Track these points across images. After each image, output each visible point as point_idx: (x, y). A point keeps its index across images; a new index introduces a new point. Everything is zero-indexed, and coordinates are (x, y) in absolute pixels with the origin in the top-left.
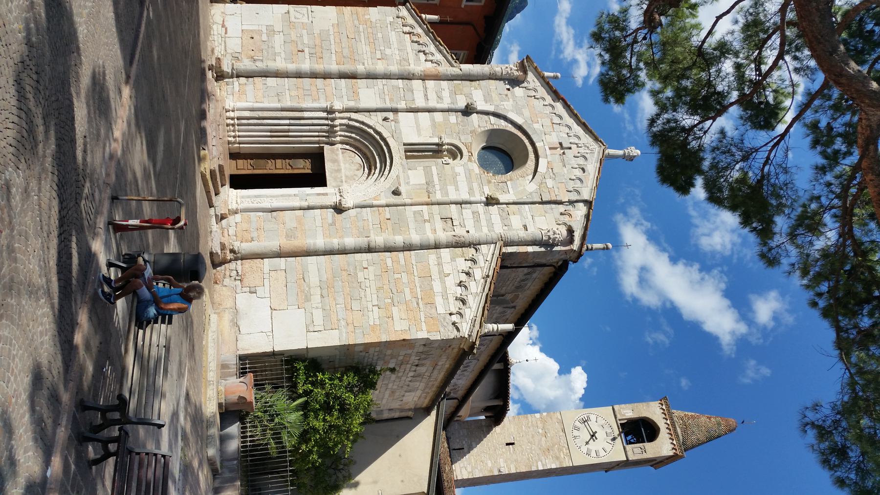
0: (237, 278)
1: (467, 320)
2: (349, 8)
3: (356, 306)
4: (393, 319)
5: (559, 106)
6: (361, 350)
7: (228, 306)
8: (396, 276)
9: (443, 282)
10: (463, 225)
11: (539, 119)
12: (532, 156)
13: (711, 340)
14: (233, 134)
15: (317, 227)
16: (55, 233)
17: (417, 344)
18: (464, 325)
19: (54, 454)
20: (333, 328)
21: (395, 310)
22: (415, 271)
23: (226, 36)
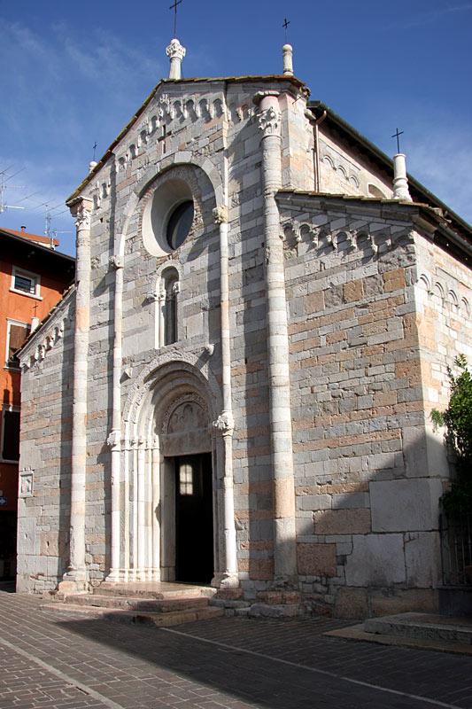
0: (324, 582)
1: (386, 226)
2: (22, 426)
3: (364, 403)
4: (386, 343)
5: (118, 152)
6: (436, 392)
7: (364, 598)
8: (323, 342)
9: (333, 271)
10: (255, 253)
11: (133, 174)
12: (173, 175)
13: (419, 232)
14: (150, 573)
15: (255, 465)
16: (458, 263)
17: (427, 304)
18: (394, 230)
19: (444, 449)
20: (350, 540)
21: (372, 341)
22: (316, 315)
23: (46, 574)
